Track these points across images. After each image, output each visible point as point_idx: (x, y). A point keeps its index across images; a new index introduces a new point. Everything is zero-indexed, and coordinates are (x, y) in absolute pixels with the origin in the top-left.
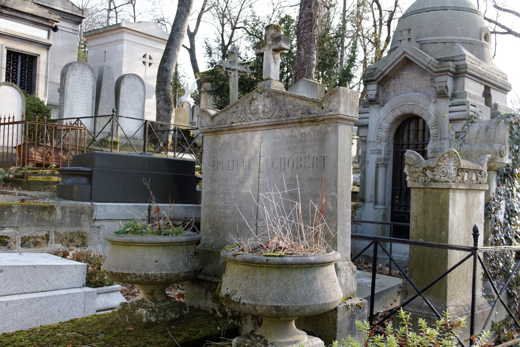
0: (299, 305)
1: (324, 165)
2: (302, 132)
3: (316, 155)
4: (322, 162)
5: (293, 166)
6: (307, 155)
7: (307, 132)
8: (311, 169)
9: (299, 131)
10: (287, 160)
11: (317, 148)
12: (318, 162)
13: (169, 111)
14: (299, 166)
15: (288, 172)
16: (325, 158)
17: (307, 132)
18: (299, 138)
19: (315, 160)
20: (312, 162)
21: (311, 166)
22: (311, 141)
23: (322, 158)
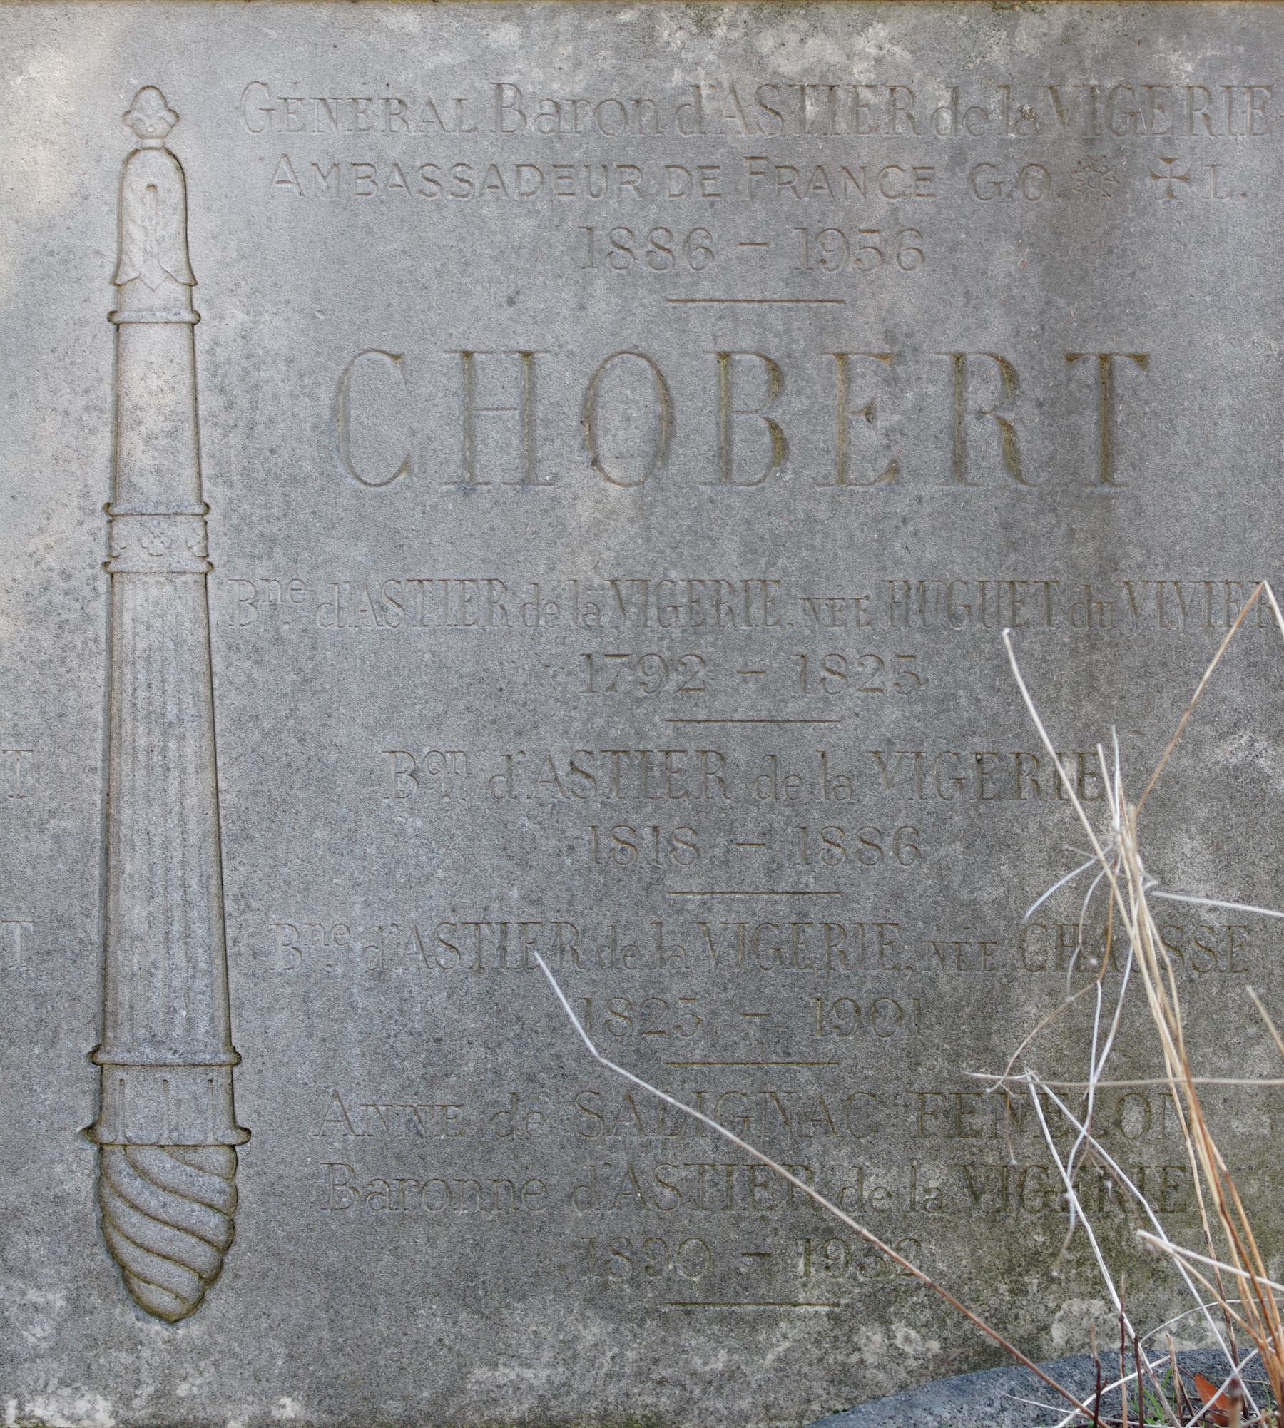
0: (970, 380)
1: (1108, 454)
2: (789, 67)
3: (997, 333)
4: (1088, 422)
5: (660, 453)
6: (863, 331)
7: (861, 72)
8: (932, 489)
9: (752, 58)
10: (561, 384)
11: (1005, 260)
12: (1026, 416)
13: (334, 411)
14: (751, 446)
15: (585, 512)
16: (1128, 373)
17: (861, 72)
18: (744, 131)
19: (982, 393)
20: (939, 414)
21: (935, 456)
22: (923, 175)
23: (1087, 372)
